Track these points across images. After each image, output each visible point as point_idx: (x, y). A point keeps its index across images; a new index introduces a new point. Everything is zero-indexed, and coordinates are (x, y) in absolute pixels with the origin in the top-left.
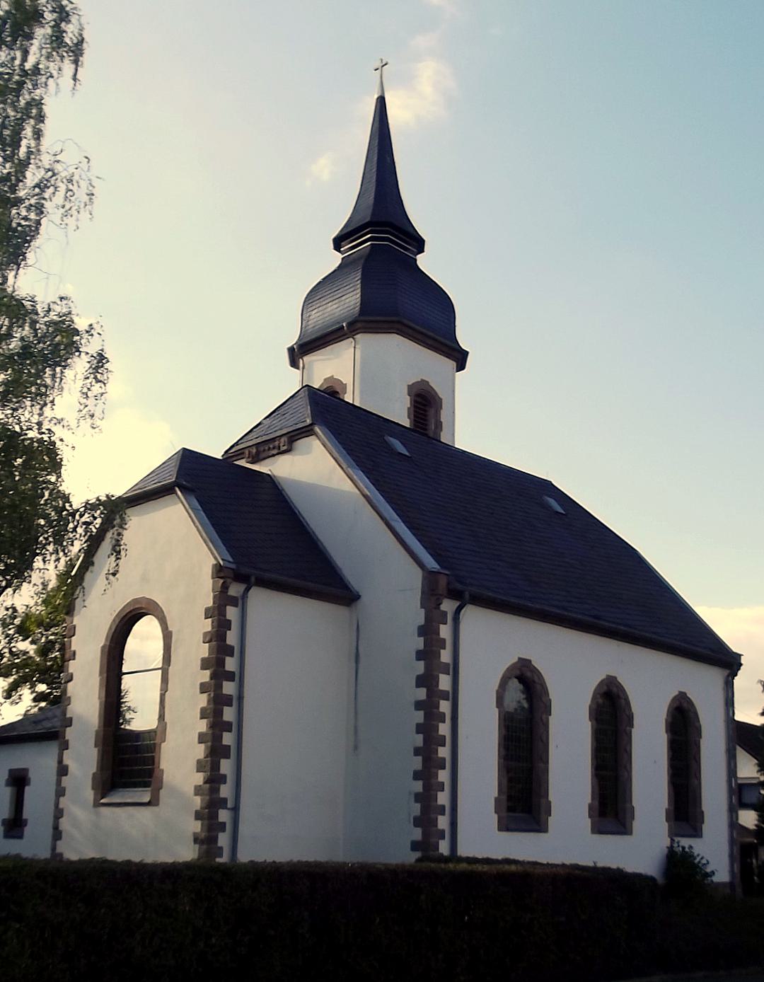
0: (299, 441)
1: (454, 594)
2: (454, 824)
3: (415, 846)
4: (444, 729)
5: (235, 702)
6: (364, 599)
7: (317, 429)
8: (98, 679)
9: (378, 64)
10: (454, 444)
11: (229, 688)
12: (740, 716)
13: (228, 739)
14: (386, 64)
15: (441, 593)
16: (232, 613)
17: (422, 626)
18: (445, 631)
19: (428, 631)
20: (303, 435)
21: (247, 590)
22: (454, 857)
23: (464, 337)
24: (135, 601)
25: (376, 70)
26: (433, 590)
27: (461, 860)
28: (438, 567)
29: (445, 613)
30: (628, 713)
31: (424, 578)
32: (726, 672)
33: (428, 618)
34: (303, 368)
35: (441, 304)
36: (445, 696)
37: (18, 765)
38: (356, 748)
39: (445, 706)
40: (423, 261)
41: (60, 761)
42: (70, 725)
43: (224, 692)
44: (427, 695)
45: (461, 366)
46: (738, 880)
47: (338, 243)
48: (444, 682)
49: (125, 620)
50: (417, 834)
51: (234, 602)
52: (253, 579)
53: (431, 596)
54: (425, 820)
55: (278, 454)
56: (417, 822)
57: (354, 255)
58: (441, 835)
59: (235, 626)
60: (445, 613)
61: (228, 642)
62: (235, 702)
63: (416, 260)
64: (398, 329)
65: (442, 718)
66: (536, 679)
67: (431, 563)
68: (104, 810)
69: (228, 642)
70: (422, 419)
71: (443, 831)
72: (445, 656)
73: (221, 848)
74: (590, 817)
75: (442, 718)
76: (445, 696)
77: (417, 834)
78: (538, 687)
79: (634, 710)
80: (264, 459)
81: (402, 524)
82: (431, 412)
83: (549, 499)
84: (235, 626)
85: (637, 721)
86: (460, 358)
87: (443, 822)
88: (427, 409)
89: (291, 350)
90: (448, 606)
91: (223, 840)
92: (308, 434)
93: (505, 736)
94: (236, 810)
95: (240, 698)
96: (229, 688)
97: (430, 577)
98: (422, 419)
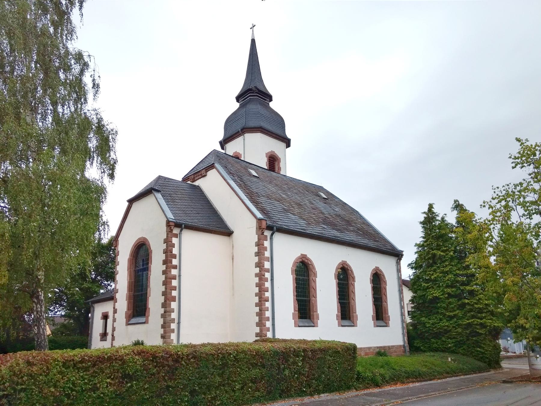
0: (209, 171)
1: (269, 228)
2: (273, 325)
3: (257, 335)
4: (268, 285)
5: (177, 278)
6: (234, 235)
7: (217, 165)
8: (127, 272)
9: (251, 26)
10: (286, 174)
11: (174, 272)
12: (403, 278)
13: (174, 293)
14: (255, 26)
15: (263, 228)
16: (175, 240)
17: (257, 242)
18: (267, 244)
19: (259, 244)
20: (211, 169)
21: (181, 231)
22: (274, 340)
23: (289, 133)
24: (140, 239)
25: (251, 29)
26: (260, 227)
27: (279, 341)
28: (263, 217)
29: (266, 236)
30: (352, 276)
31: (257, 222)
32: (397, 258)
33: (259, 239)
34: (226, 149)
35: (280, 121)
36: (267, 271)
37: (105, 311)
38: (233, 295)
39: (268, 275)
40: (271, 105)
41: (114, 308)
42: (117, 292)
43: (172, 274)
44: (260, 271)
45: (288, 145)
46: (407, 345)
47: (238, 99)
48: (267, 265)
49: (136, 247)
50: (257, 330)
51: (176, 236)
52: (183, 226)
53: (260, 229)
54: (261, 324)
55: (202, 177)
56: (258, 325)
57: (243, 104)
58: (268, 330)
59: (177, 246)
60: (266, 236)
61: (174, 252)
62: (177, 278)
63: (269, 104)
64: (261, 131)
65: (266, 280)
66: (309, 263)
67: (259, 215)
68: (129, 327)
69: (174, 252)
70: (273, 168)
71: (269, 328)
72: (267, 254)
73: (173, 340)
74: (337, 319)
75: (266, 280)
76: (267, 271)
77: (257, 330)
78: (311, 266)
79: (355, 275)
80: (197, 180)
81: (249, 201)
82: (276, 163)
83: (320, 193)
84: (177, 246)
85: (357, 279)
86: (287, 142)
87: (269, 324)
88: (275, 162)
89: (221, 143)
90: (267, 233)
91: (173, 336)
92: (212, 168)
93: (296, 287)
94: (179, 323)
95: (180, 276)
96: (174, 272)
97: (259, 220)
98: (273, 168)
